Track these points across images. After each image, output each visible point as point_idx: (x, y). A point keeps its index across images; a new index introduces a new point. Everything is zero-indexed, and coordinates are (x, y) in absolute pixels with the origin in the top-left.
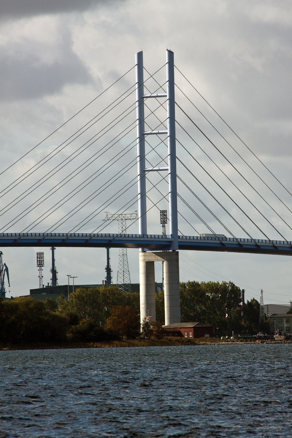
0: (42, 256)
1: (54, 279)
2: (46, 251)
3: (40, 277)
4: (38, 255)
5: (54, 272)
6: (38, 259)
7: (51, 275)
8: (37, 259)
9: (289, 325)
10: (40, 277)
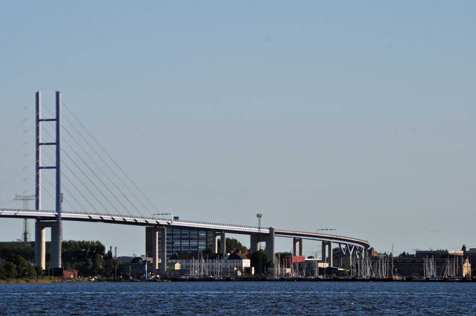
1: (25, 238)
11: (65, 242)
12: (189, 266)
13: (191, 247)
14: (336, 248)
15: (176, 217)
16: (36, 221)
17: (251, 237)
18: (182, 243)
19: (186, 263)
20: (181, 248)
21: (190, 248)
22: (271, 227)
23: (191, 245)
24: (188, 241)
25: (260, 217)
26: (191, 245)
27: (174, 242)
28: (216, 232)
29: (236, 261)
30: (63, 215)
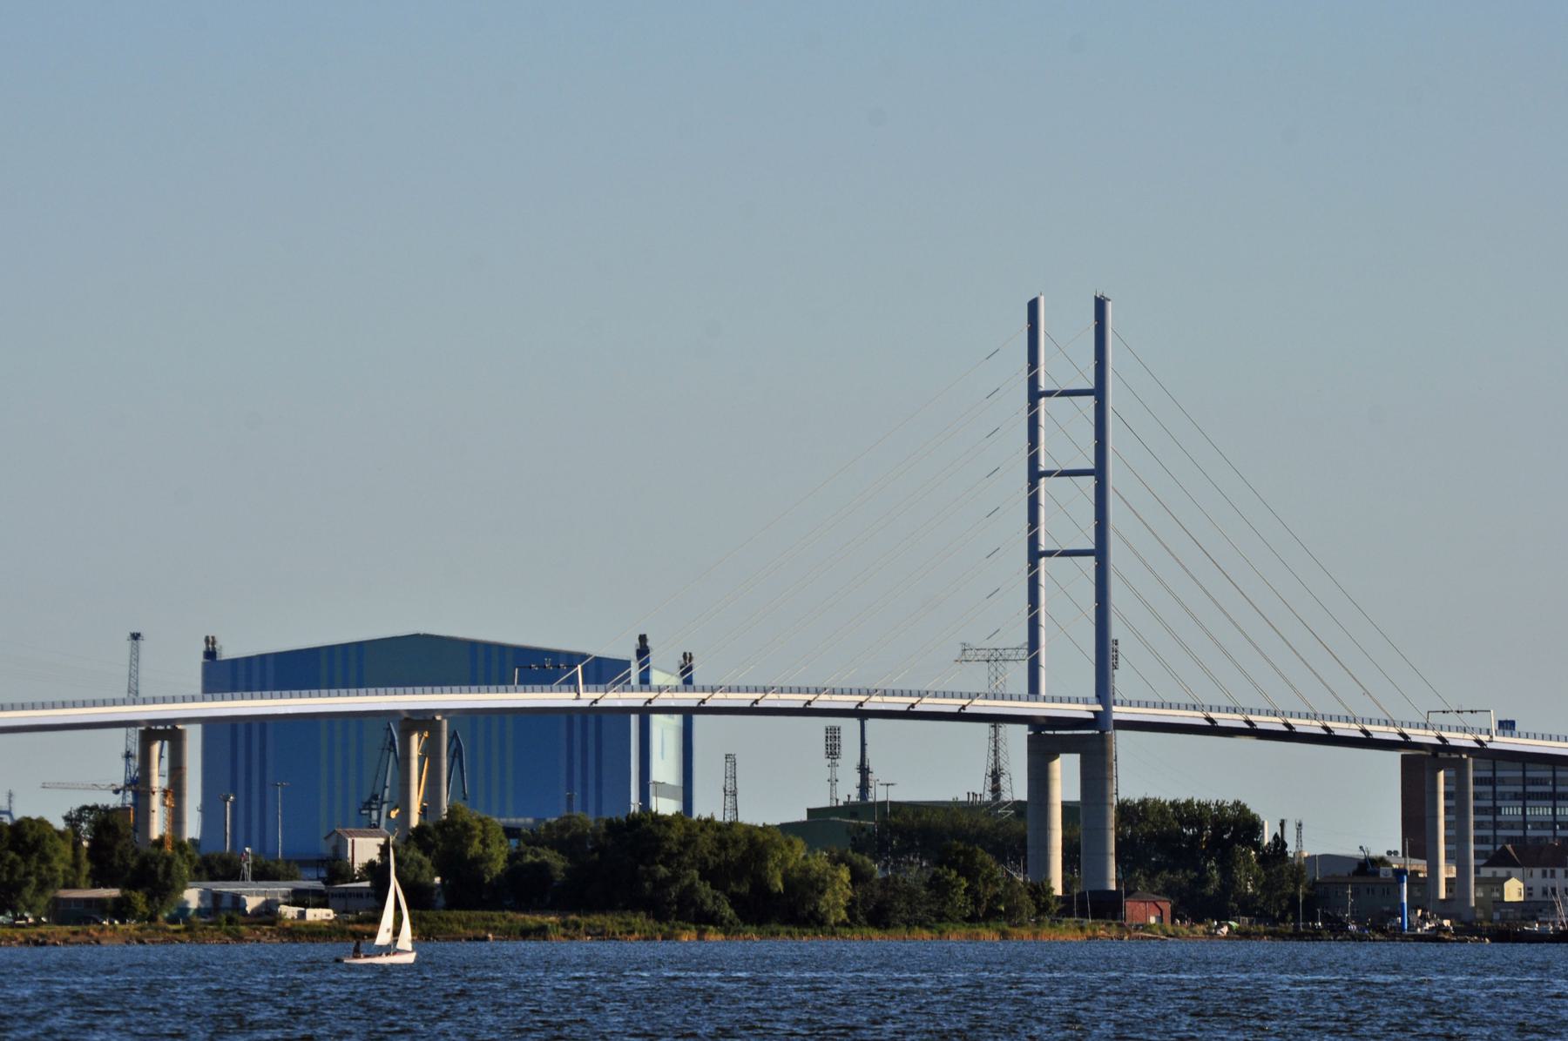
0: (837, 735)
1: (864, 787)
2: (850, 726)
3: (833, 782)
4: (827, 733)
5: (864, 770)
6: (829, 742)
7: (856, 778)
8: (827, 741)
9: (699, 833)
10: (833, 782)
12: (1554, 890)
13: (1559, 823)
14: (72, 820)
15: (1506, 722)
16: (1031, 733)
18: (1558, 810)
19: (1545, 879)
20: (1525, 828)
21: (1558, 827)
23: (1558, 819)
24: (1550, 803)
26: (1558, 819)
27: (1500, 808)
30: (1120, 713)
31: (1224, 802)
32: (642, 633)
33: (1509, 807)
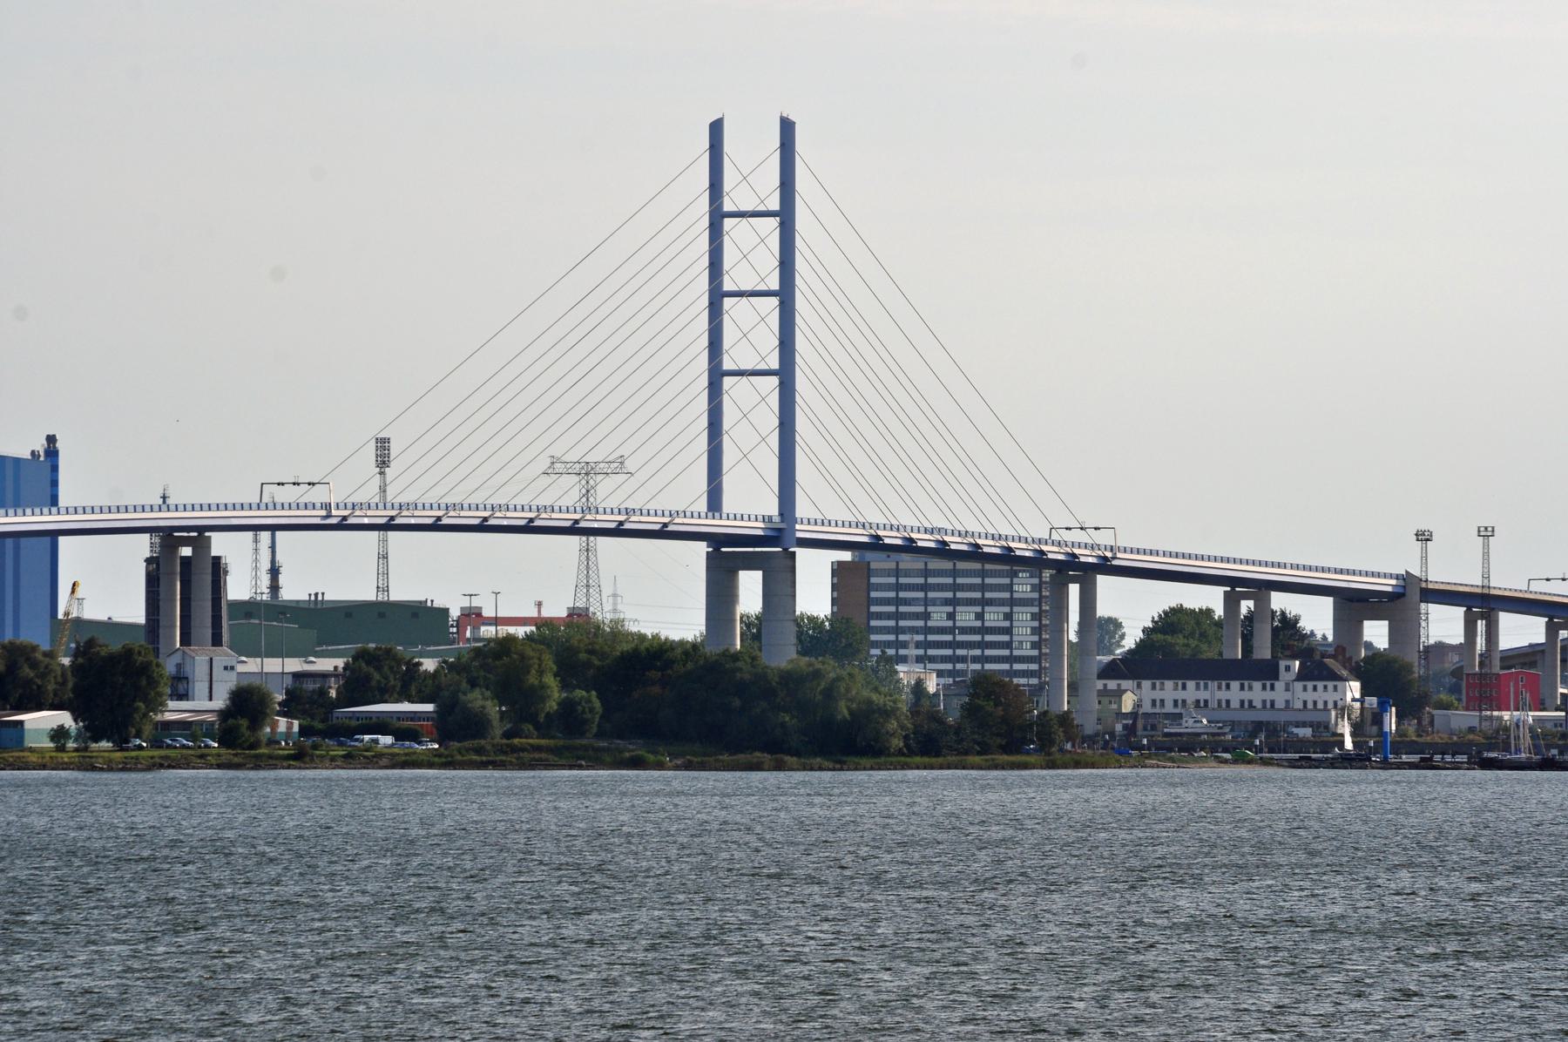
5: (274, 572)
11: (429, 604)
12: (1162, 701)
16: (710, 549)
17: (1335, 603)
19: (1264, 692)
22: (1407, 572)
25: (1428, 540)
28: (723, 549)
29: (1325, 687)
30: (802, 530)
31: (316, 595)
32: (51, 433)
33: (871, 602)
